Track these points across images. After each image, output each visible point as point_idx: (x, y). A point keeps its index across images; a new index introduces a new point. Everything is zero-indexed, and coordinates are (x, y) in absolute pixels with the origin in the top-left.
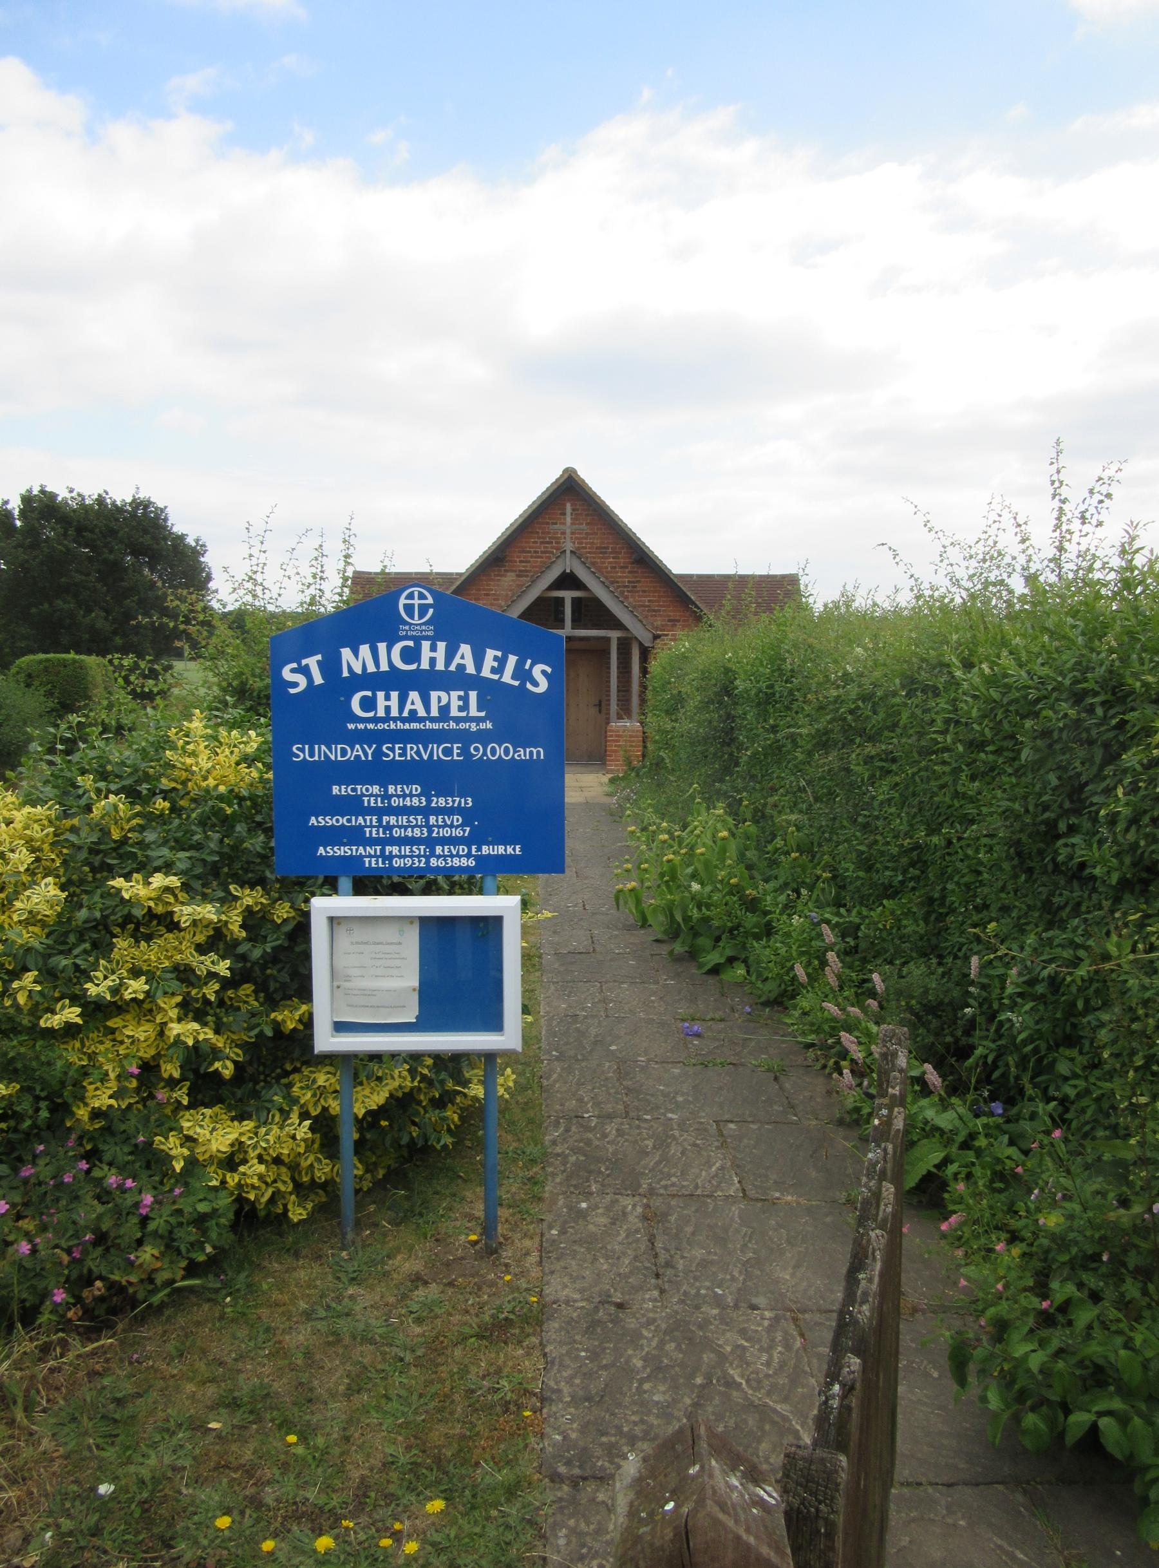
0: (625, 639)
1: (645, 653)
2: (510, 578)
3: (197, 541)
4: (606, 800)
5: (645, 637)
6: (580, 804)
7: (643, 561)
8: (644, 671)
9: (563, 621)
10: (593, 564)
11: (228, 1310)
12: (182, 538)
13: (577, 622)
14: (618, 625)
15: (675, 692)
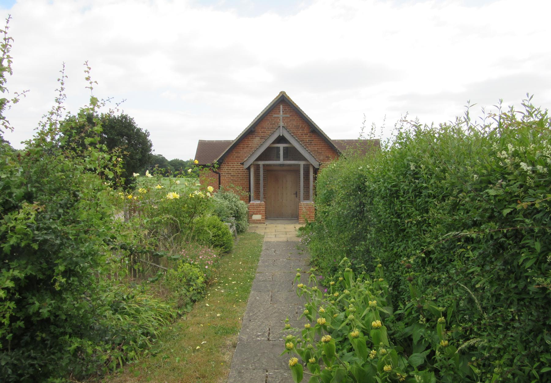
0: (307, 165)
1: (316, 171)
3: (146, 131)
8: (315, 178)
10: (293, 133)
12: (139, 130)
13: (286, 157)
14: (304, 159)
15: (329, 189)
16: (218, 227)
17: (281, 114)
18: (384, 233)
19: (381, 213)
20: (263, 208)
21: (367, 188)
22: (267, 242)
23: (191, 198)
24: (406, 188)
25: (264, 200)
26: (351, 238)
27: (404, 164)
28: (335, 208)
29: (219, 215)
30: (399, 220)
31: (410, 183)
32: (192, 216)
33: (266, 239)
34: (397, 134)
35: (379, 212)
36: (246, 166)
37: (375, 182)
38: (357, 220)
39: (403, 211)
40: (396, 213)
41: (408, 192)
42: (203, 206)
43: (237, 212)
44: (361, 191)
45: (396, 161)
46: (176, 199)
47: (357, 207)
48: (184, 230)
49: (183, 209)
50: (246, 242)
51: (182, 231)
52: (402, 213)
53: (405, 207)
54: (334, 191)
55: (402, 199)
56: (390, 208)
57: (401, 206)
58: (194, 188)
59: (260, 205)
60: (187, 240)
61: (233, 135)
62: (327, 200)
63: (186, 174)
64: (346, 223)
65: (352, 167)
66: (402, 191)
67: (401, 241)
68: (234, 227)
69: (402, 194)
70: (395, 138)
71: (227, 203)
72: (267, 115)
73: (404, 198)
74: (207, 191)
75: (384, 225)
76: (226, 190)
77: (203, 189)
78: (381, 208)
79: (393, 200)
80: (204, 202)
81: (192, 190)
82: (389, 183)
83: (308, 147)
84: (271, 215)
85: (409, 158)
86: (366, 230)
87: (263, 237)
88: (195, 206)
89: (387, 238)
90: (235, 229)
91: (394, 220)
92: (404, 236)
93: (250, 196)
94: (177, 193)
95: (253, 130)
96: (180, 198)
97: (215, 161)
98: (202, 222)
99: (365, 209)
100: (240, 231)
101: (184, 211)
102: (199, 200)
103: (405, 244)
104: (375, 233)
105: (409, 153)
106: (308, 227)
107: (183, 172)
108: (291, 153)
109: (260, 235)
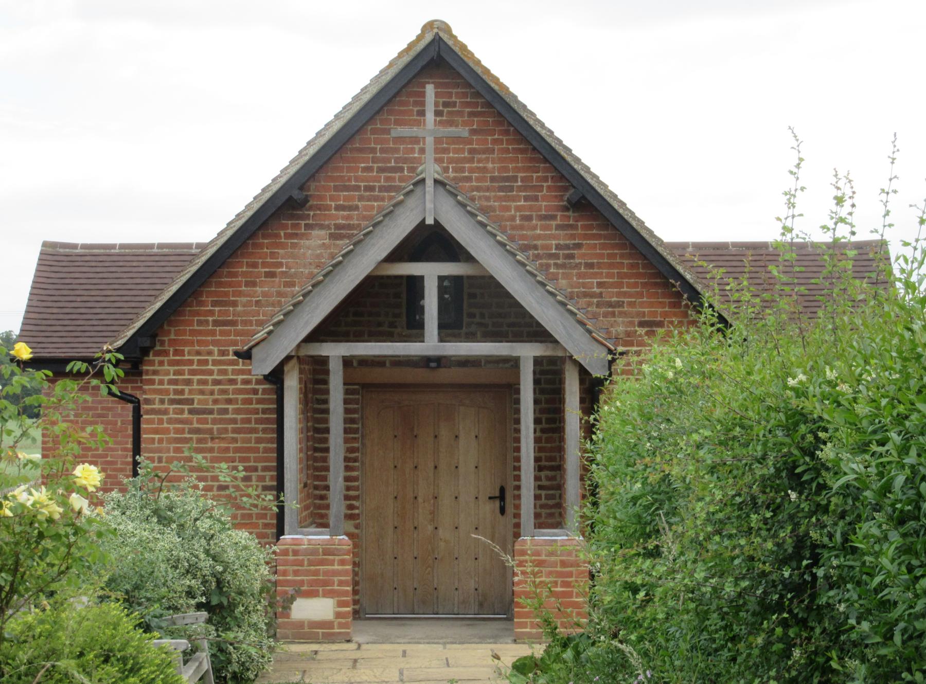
0: (552, 360)
1: (592, 391)
5: (592, 358)
7: (588, 204)
8: (589, 430)
9: (421, 326)
11: (796, 351)
13: (450, 328)
14: (539, 334)
15: (654, 478)
16: (124, 660)
17: (429, 123)
19: (893, 593)
20: (341, 568)
21: (827, 476)
25: (349, 526)
29: (130, 601)
35: (883, 585)
36: (264, 364)
37: (863, 448)
38: (785, 624)
43: (219, 582)
44: (800, 487)
47: (783, 562)
54: (678, 485)
59: (326, 552)
61: (203, 221)
62: (643, 534)
64: (733, 639)
65: (755, 377)
68: (204, 660)
71: (168, 540)
77: (56, 478)
78: (893, 568)
83: (554, 278)
90: (206, 665)
93: (281, 508)
95: (296, 194)
98: (50, 635)
99: (820, 573)
106: (558, 659)
108: (479, 305)
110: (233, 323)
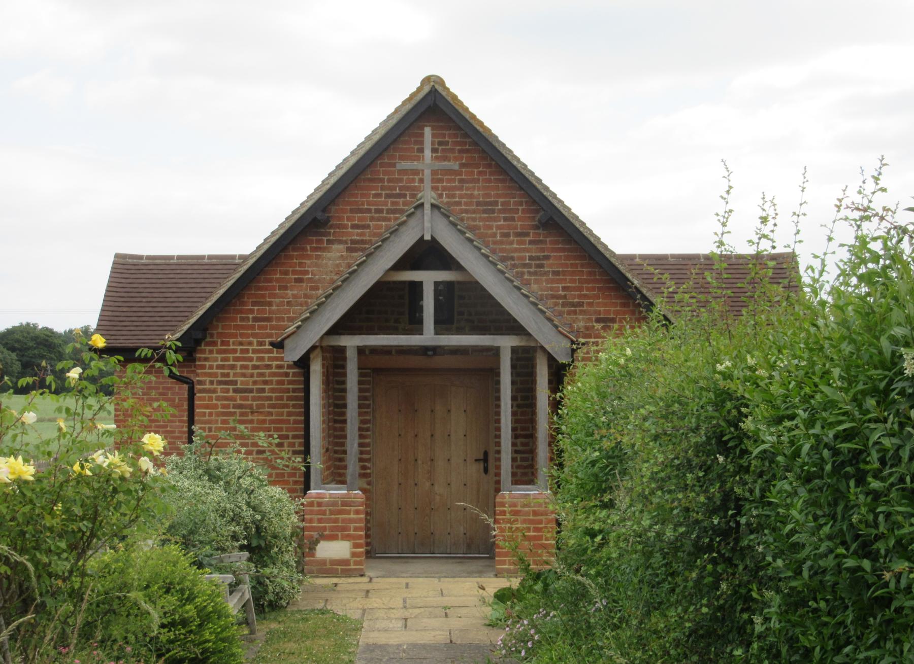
2: (337, 251)
4: (484, 636)
5: (558, 347)
6: (435, 647)
13: (444, 323)
14: (513, 327)
17: (427, 156)
18: (816, 610)
20: (356, 517)
21: (748, 443)
22: (371, 648)
23: (81, 479)
24: (887, 442)
25: (363, 483)
26: (693, 632)
27: (881, 353)
28: (630, 518)
29: (187, 544)
30: (866, 564)
31: (902, 425)
32: (80, 546)
33: (367, 637)
34: (852, 241)
35: (793, 532)
36: (294, 353)
38: (714, 561)
39: (882, 529)
40: (858, 536)
41: (897, 460)
42: (124, 509)
43: (258, 529)
44: (726, 452)
45: (852, 341)
46: (21, 483)
47: (714, 512)
48: (49, 602)
49: (48, 521)
50: (292, 646)
51: (43, 605)
52: (877, 538)
53: (888, 515)
54: (630, 452)
55: (875, 484)
56: (834, 517)
57: (872, 510)
58: (91, 438)
59: (344, 504)
60: (62, 640)
62: (599, 487)
63: (62, 389)
64: (673, 574)
66: (875, 455)
67: (876, 645)
68: (246, 591)
69: (877, 465)
70: (845, 255)
71: (217, 494)
72: (372, 163)
73: (883, 480)
74: (139, 453)
75: (815, 583)
76: (217, 446)
77: (127, 443)
78: (800, 517)
79: (842, 487)
80: (128, 492)
81: (84, 449)
82: (826, 425)
83: (527, 283)
84: (391, 541)
85: (898, 331)
86: (748, 599)
87: (358, 629)
88: (92, 510)
89: (827, 632)
90: (248, 595)
91: (850, 563)
92: (889, 622)
93: (308, 468)
94: (26, 461)
95: (319, 215)
96: (39, 480)
97: (171, 338)
98: (122, 572)
100: (266, 603)
101: (51, 529)
102: (107, 487)
103: (892, 654)
104: (782, 614)
105: (897, 315)
106: (531, 590)
107: (49, 379)
108: (464, 305)
109: (344, 620)
110: (268, 319)
